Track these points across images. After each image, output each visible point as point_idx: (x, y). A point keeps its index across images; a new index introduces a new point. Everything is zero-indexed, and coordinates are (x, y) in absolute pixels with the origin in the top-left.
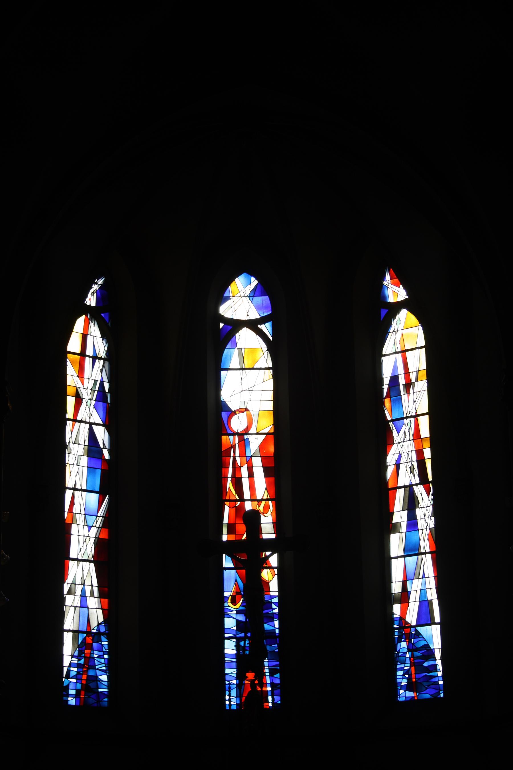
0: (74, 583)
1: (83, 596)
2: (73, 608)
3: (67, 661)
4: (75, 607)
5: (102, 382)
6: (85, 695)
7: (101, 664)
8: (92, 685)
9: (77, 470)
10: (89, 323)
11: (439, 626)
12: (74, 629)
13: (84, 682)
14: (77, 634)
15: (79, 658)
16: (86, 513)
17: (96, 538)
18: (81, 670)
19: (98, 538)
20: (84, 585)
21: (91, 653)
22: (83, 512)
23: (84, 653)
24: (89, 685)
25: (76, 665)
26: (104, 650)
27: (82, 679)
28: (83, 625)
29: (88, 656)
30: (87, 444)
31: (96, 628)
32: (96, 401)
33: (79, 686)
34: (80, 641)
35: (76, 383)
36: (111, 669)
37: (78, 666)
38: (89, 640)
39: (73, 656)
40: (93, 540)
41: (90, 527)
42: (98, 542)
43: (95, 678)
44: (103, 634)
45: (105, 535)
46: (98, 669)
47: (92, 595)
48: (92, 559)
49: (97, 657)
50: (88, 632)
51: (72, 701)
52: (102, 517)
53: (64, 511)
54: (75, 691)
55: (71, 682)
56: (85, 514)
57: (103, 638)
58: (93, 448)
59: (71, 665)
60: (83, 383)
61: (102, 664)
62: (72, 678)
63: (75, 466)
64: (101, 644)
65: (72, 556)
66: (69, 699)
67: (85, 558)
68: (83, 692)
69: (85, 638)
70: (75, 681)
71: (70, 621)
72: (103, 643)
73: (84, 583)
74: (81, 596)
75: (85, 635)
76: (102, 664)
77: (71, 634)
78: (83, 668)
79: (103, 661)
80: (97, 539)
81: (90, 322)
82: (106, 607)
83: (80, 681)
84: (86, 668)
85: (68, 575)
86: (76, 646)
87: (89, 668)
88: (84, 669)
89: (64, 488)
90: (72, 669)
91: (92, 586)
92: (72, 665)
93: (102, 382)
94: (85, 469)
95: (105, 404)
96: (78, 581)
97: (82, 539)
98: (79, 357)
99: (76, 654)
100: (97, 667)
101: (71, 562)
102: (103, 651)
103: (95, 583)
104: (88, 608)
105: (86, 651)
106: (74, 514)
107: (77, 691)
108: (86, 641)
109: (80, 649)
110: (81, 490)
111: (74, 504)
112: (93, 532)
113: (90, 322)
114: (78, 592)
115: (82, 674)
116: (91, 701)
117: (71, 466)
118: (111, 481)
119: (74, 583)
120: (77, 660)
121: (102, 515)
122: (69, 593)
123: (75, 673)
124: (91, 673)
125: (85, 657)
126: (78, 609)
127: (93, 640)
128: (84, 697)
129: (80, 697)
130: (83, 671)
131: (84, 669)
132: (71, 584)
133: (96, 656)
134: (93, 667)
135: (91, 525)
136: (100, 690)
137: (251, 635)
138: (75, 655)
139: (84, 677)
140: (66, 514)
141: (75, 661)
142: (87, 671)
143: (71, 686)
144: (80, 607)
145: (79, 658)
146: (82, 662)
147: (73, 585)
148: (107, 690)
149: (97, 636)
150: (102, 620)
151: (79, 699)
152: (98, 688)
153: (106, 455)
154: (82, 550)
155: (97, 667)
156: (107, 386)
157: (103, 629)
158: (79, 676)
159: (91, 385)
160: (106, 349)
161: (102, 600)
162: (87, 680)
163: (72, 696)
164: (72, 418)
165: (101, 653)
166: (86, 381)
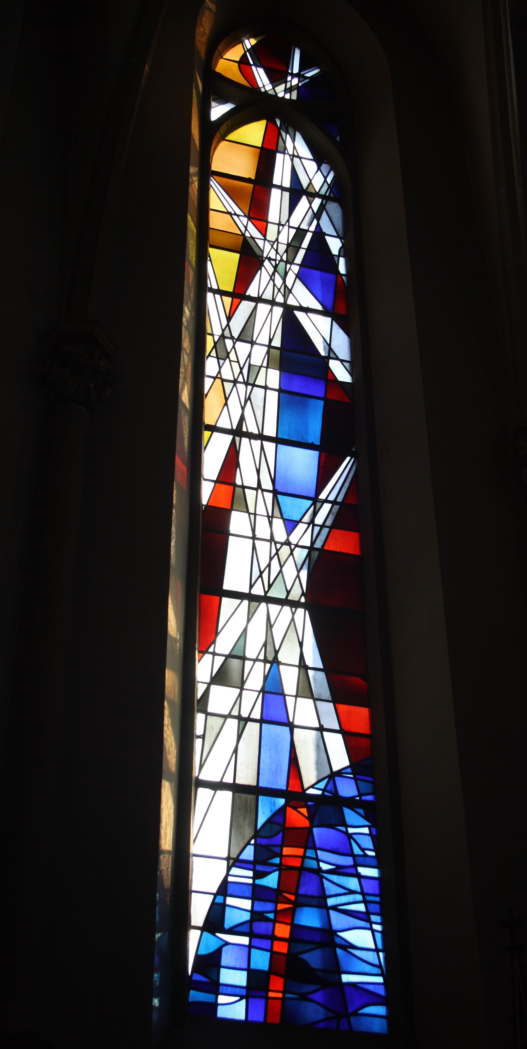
1: (272, 690)
2: (232, 724)
3: (206, 876)
4: (243, 721)
5: (319, 235)
6: (284, 992)
7: (347, 893)
8: (314, 958)
12: (241, 780)
13: (281, 948)
14: (251, 797)
15: (259, 868)
16: (279, 488)
17: (311, 549)
18: (269, 906)
20: (275, 662)
21: (304, 857)
22: (267, 484)
23: (281, 855)
24: (305, 962)
25: (221, 989)
26: (357, 851)
27: (273, 938)
28: (276, 773)
29: (296, 863)
30: (277, 342)
32: (301, 266)
33: (261, 960)
34: (262, 820)
35: (243, 229)
36: (391, 904)
37: (257, 893)
38: (298, 818)
39: (234, 862)
40: (301, 554)
41: (291, 525)
42: (321, 563)
43: (328, 938)
44: (351, 803)
46: (335, 908)
47: (305, 690)
48: (303, 600)
49: (329, 872)
50: (294, 795)
51: (232, 1009)
52: (334, 503)
54: (245, 973)
55: (227, 944)
56: (275, 492)
57: (350, 816)
59: (224, 889)
60: (264, 232)
61: (351, 892)
62: (232, 931)
63: (241, 387)
64: (346, 833)
65: (227, 585)
66: (222, 999)
68: (277, 983)
69: (283, 809)
70: (245, 940)
71: (225, 752)
72: (351, 830)
73: (276, 657)
74: (263, 691)
76: (351, 892)
77: (226, 797)
78: (276, 902)
79: (353, 883)
80: (315, 554)
81: (283, 134)
83: (266, 943)
84: (288, 901)
85: (217, 634)
86: (249, 832)
87: (298, 904)
88: (281, 906)
90: (230, 901)
91: (303, 666)
92: (230, 890)
93: (319, 235)
94: (273, 397)
95: (332, 277)
97: (264, 549)
98: (251, 186)
99: (249, 854)
100: (331, 902)
101: (225, 600)
102: (351, 854)
103: (313, 658)
104: (291, 726)
105: (286, 851)
106: (239, 490)
107: (252, 974)
108: (284, 826)
109: (264, 842)
110: (261, 437)
111: (238, 465)
112: (302, 535)
113: (283, 134)
114: (256, 677)
115: (274, 921)
116: (313, 1012)
117: (228, 386)
120: (250, 873)
121: (331, 498)
122: (220, 678)
123: (246, 917)
124: (309, 918)
125: (280, 868)
126: (252, 729)
127: (310, 818)
128: (283, 999)
129: (267, 998)
130: (276, 912)
131: (281, 906)
132: (227, 657)
133: (325, 867)
134: (320, 901)
135: (297, 518)
136: (346, 978)
137: (160, 1002)
138: (244, 856)
139: (283, 931)
141: (243, 876)
142: (291, 913)
143: (227, 958)
144: (261, 721)
145: (259, 868)
146: (271, 881)
147: (235, 663)
148: (380, 980)
149: (328, 807)
151: (261, 1003)
152: (341, 972)
153: (341, 373)
154: (265, 575)
155: (331, 902)
157: (347, 789)
158: (261, 927)
159: (286, 236)
160: (329, 180)
161: (342, 707)
162: (289, 941)
163: (232, 990)
165: (348, 861)
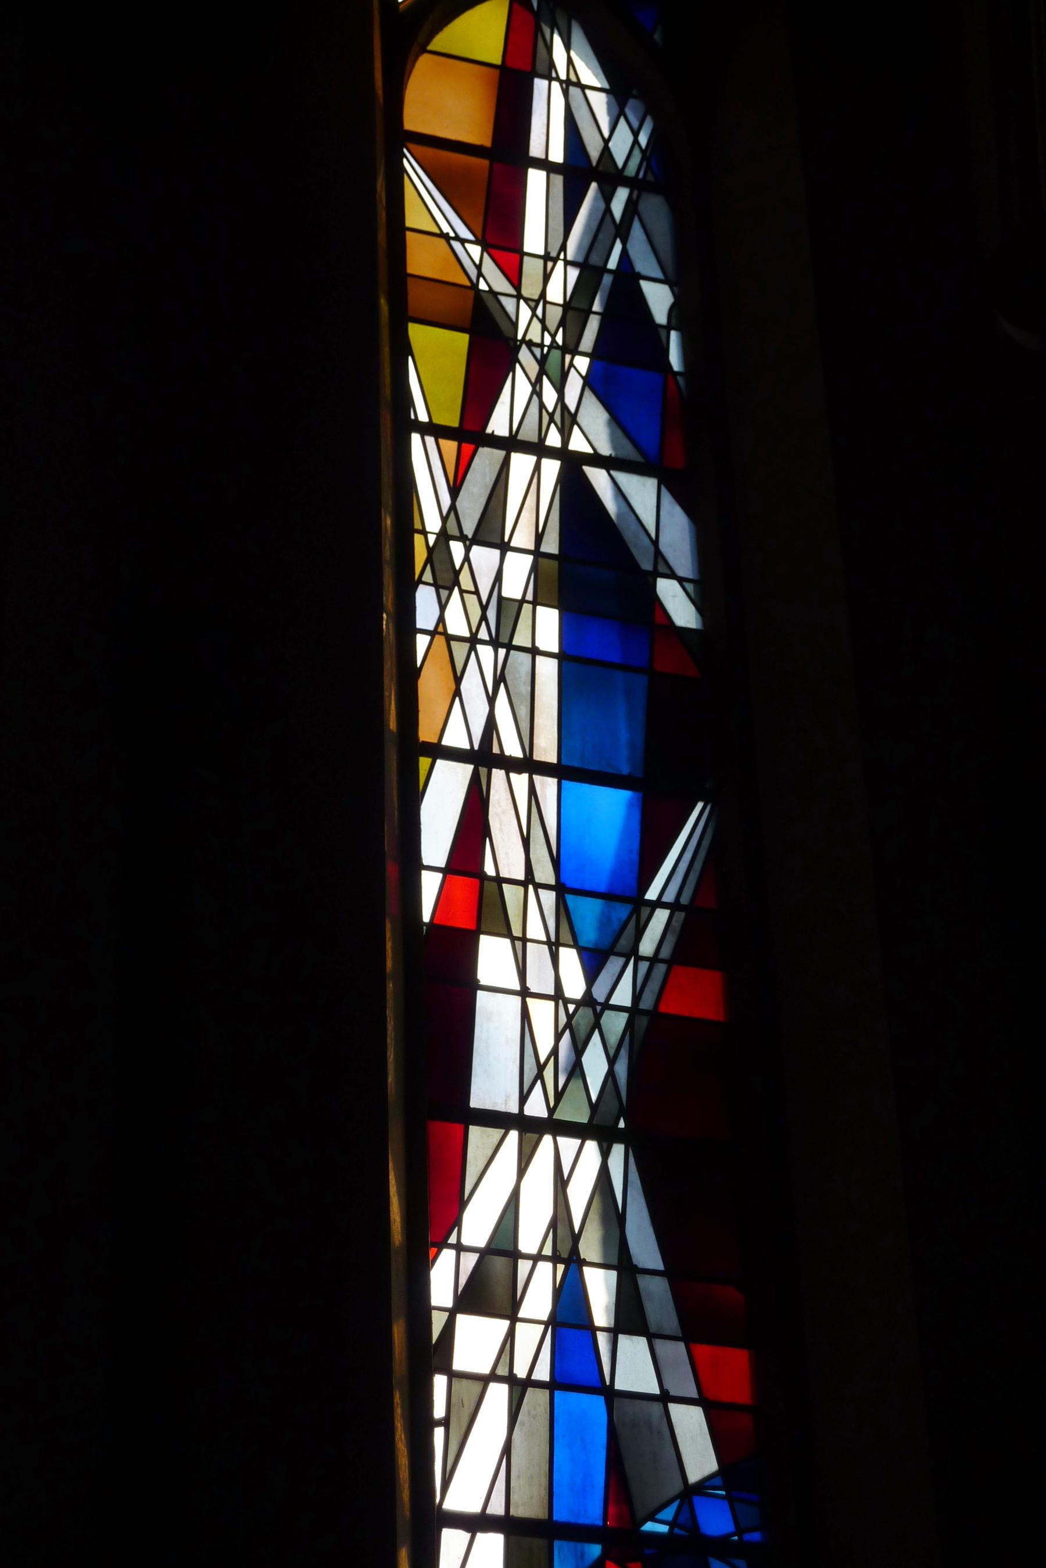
0: (503, 1246)
1: (569, 1315)
2: (498, 1394)
4: (519, 1387)
9: (490, 688)
10: (538, 30)
11: (419, 626)
12: (516, 1512)
14: (539, 1543)
16: (570, 881)
19: (654, 1014)
22: (545, 873)
30: (551, 545)
31: (668, 1514)
45: (703, 999)
47: (630, 1317)
52: (674, 907)
53: (604, 316)
56: (561, 889)
58: (590, 563)
65: (481, 1097)
67: (575, 1111)
73: (575, 1250)
75: (595, 1550)
80: (643, 1022)
82: (738, 1389)
89: (417, 751)
96: (531, 1236)
98: (485, 163)
110: (529, 765)
114: (538, 1299)
118: (655, 708)
119: (503, 1246)
121: (669, 897)
122: (475, 1297)
126: (536, 1401)
140: (430, 885)
147: (499, 1263)
150: (711, 1465)
154: (549, 1073)
156: (659, 299)
161: (703, 1350)
164: (455, 423)
166: (532, 269)
